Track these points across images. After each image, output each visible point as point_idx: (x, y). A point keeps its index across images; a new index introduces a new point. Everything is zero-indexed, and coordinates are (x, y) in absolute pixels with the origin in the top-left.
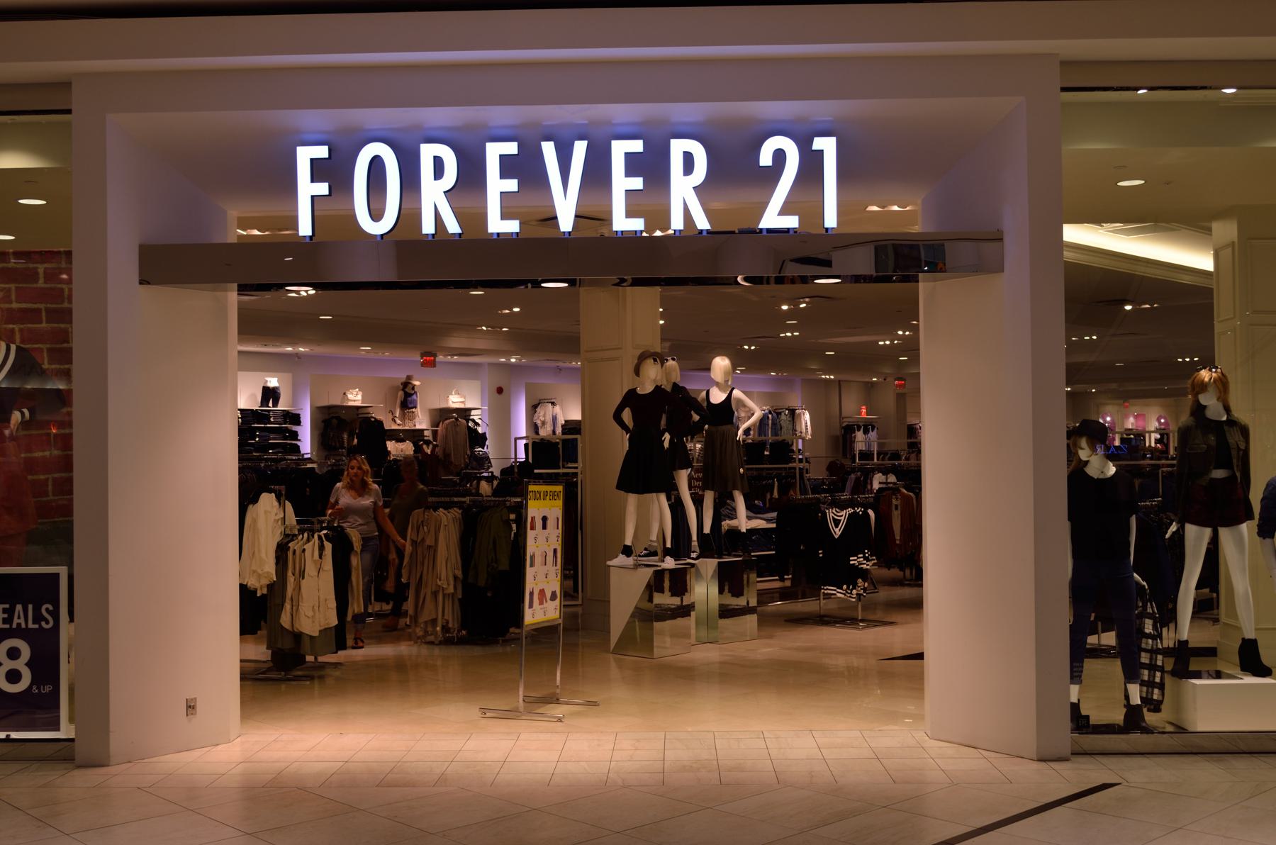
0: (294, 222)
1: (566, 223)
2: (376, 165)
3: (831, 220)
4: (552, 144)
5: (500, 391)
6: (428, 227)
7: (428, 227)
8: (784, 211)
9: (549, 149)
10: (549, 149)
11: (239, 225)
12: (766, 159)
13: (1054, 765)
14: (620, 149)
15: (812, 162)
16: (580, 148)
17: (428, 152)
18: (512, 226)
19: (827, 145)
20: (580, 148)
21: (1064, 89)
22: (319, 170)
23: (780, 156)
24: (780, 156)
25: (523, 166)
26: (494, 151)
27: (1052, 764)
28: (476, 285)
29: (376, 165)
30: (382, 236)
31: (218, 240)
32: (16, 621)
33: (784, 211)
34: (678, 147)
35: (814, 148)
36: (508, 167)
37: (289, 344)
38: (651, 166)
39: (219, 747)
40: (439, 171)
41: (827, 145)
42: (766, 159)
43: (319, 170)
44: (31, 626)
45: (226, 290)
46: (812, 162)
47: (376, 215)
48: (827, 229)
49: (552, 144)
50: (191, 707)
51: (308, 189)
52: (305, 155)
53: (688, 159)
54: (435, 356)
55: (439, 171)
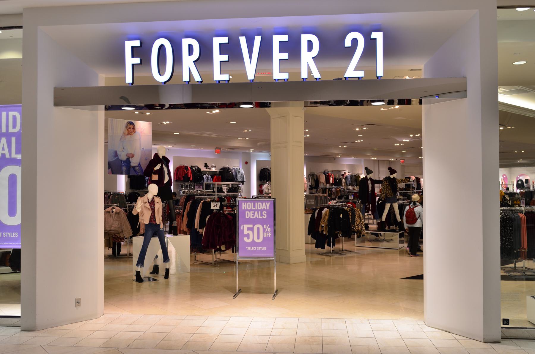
0: (124, 78)
1: (251, 76)
2: (162, 48)
3: (380, 73)
4: (244, 37)
5: (246, 163)
6: (186, 78)
7: (186, 78)
8: (357, 69)
9: (243, 40)
10: (243, 40)
11: (102, 78)
12: (348, 43)
13: (492, 345)
14: (277, 40)
15: (370, 45)
16: (258, 40)
17: (186, 42)
18: (225, 77)
19: (378, 36)
20: (258, 40)
21: (499, 7)
22: (135, 52)
23: (355, 41)
24: (355, 41)
25: (232, 50)
26: (217, 42)
27: (490, 344)
28: (212, 106)
29: (162, 48)
30: (165, 83)
31: (94, 85)
32: (255, 216)
33: (357, 69)
34: (305, 38)
35: (372, 37)
36: (223, 49)
37: (165, 144)
38: (292, 48)
39: (91, 321)
40: (191, 52)
41: (378, 36)
42: (348, 43)
43: (135, 52)
44: (260, 217)
45: (97, 110)
46: (370, 45)
47: (161, 72)
48: (378, 77)
49: (244, 37)
50: (78, 302)
51: (130, 60)
52: (129, 45)
53: (310, 43)
54: (220, 149)
55: (191, 52)
